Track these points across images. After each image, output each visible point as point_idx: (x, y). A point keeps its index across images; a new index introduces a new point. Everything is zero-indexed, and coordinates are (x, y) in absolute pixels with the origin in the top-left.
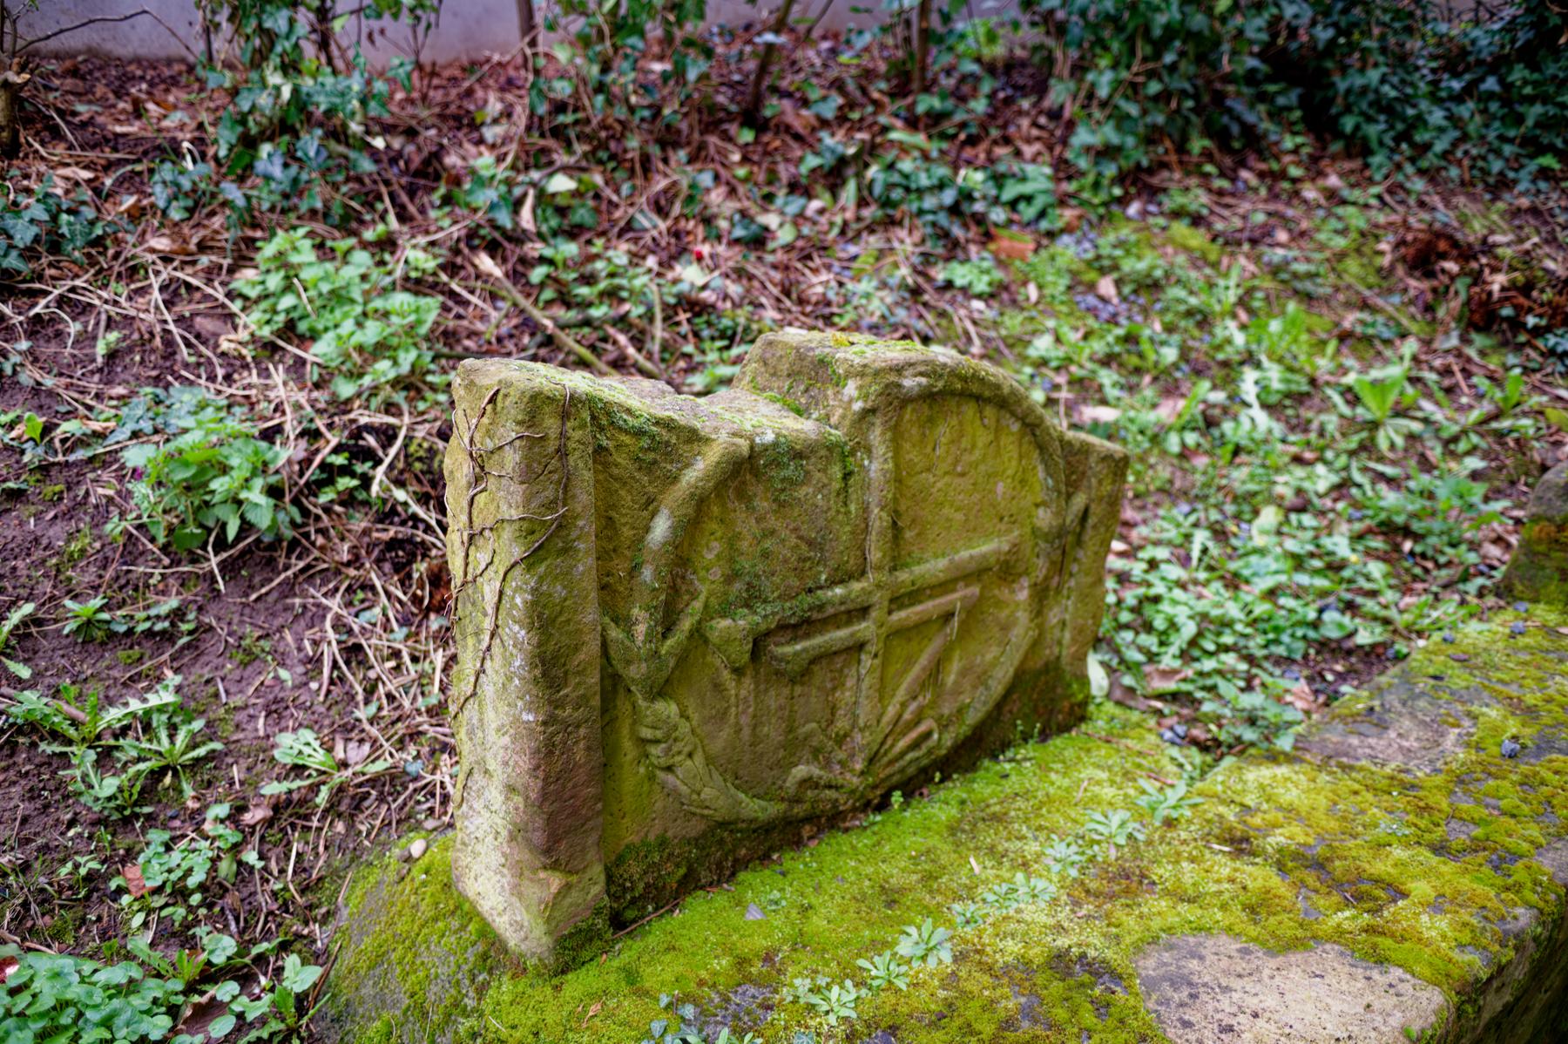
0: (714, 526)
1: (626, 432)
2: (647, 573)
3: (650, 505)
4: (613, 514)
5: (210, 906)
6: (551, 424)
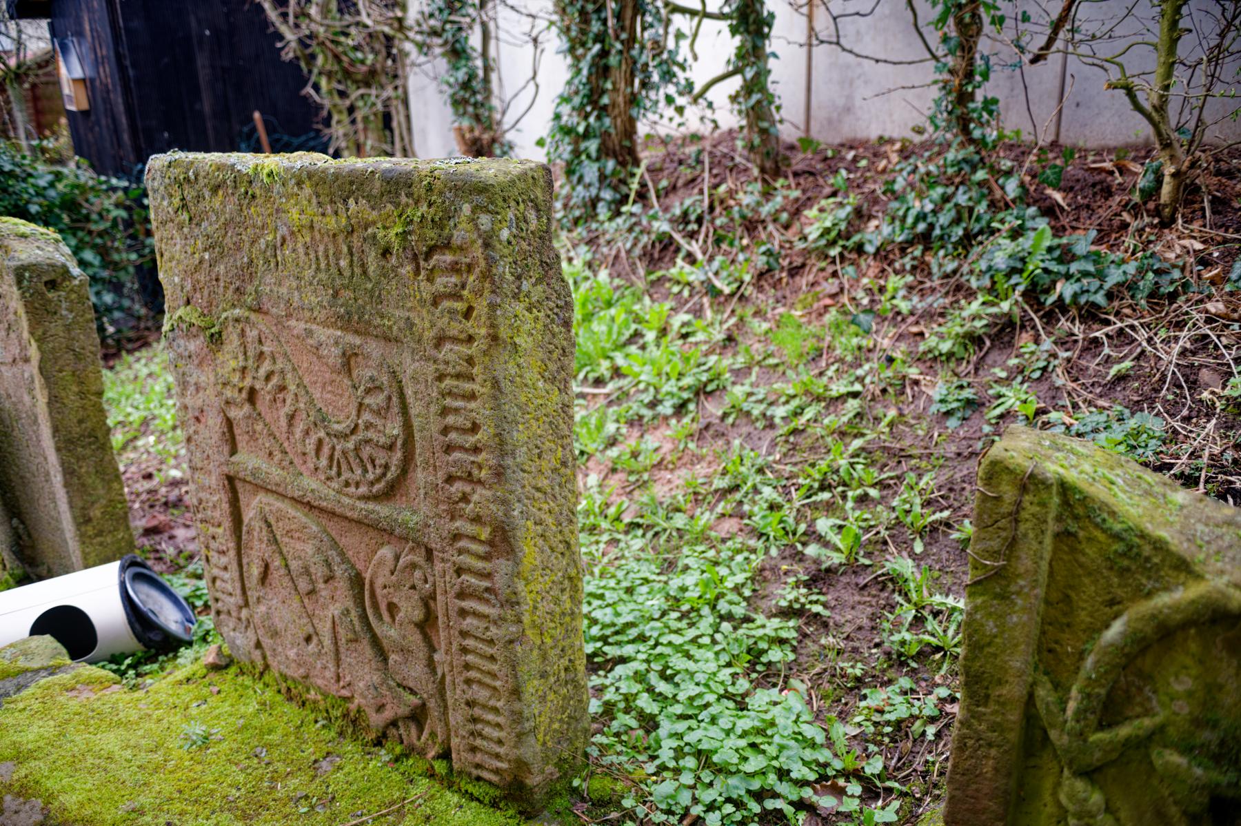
0: (1189, 661)
1: (1104, 531)
2: (1089, 661)
3: (1114, 605)
4: (1073, 594)
5: (893, 740)
6: (1008, 492)
